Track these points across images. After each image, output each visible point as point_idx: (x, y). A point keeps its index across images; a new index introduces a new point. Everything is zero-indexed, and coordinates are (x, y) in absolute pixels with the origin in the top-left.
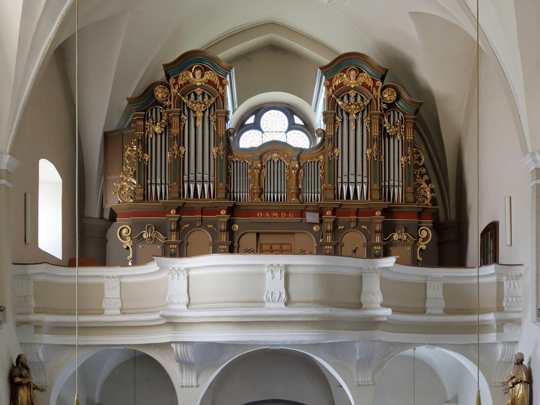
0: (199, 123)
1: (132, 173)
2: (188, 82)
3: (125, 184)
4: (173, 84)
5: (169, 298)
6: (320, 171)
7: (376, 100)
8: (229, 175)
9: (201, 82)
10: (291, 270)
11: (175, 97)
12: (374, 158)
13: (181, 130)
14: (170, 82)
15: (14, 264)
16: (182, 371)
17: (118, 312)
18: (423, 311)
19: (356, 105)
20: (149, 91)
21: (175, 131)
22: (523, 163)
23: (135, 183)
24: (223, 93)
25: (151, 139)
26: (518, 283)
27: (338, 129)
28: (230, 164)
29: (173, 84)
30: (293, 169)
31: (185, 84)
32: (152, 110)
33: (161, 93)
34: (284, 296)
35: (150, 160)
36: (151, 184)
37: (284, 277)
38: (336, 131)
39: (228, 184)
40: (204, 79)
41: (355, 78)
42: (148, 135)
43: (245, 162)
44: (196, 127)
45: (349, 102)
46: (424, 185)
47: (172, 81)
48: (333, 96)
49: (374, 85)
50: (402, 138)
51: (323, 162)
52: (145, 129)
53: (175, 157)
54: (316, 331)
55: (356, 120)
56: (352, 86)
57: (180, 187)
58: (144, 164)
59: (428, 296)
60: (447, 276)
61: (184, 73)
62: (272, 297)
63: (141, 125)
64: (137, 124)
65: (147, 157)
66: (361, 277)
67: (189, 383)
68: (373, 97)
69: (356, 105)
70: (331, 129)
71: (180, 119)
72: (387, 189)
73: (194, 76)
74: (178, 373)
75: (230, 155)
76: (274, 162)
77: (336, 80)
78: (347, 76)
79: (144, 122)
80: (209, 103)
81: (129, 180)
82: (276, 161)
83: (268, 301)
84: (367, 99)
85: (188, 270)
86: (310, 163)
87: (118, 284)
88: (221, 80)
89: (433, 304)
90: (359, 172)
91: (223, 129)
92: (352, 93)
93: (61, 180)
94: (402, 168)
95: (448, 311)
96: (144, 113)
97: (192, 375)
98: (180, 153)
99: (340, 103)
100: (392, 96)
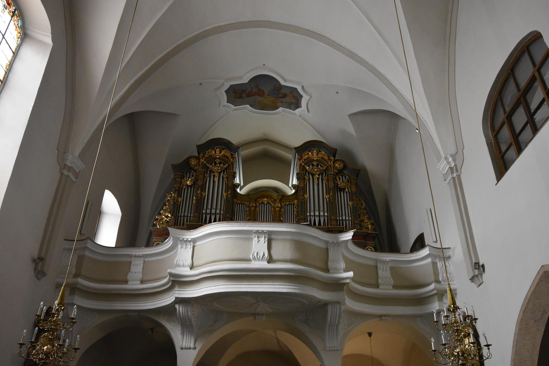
0: (216, 179)
1: (169, 210)
2: (211, 156)
3: (163, 217)
4: (202, 157)
5: (177, 261)
6: (295, 209)
7: (331, 167)
8: (234, 211)
9: (219, 156)
10: (273, 237)
11: (202, 164)
12: (331, 200)
13: (204, 182)
14: (200, 156)
15: (65, 240)
16: (183, 336)
17: (139, 282)
18: (377, 286)
19: (318, 169)
20: (187, 162)
21: (200, 183)
22: (439, 168)
23: (170, 216)
24: (233, 162)
25: (185, 189)
26: (449, 263)
27: (306, 183)
28: (234, 204)
29: (202, 157)
30: (277, 207)
31: (209, 157)
32: (187, 174)
33: (194, 162)
34: (266, 255)
35: (182, 202)
36: (181, 216)
37: (267, 241)
38: (305, 184)
39: (233, 217)
40: (221, 154)
41: (316, 154)
42: (182, 187)
43: (245, 204)
44: (214, 182)
45: (313, 167)
46: (366, 221)
47: (201, 155)
48: (303, 164)
49: (329, 159)
50: (349, 191)
51: (297, 204)
52: (181, 183)
53: (199, 198)
54: (292, 284)
55: (318, 179)
56: (315, 159)
57: (200, 217)
58: (178, 204)
59: (379, 276)
60: (392, 260)
61: (210, 151)
62: (257, 256)
63: (179, 181)
64: (177, 180)
65: (180, 199)
66: (327, 250)
67: (188, 345)
68: (328, 165)
69: (318, 169)
70: (302, 183)
71: (204, 176)
72: (341, 221)
73: (215, 152)
74: (180, 337)
75: (235, 199)
76: (264, 204)
77: (304, 156)
78: (311, 153)
79: (181, 180)
80: (223, 167)
81: (166, 215)
82: (265, 203)
83: (254, 259)
84: (325, 166)
85: (194, 241)
86: (289, 205)
87: (142, 262)
88: (232, 155)
89: (384, 281)
90: (322, 209)
91: (231, 182)
92: (315, 163)
93: (121, 214)
94: (350, 209)
95: (395, 287)
96: (181, 174)
97: (191, 339)
98: (202, 195)
99: (307, 168)
100: (341, 165)
